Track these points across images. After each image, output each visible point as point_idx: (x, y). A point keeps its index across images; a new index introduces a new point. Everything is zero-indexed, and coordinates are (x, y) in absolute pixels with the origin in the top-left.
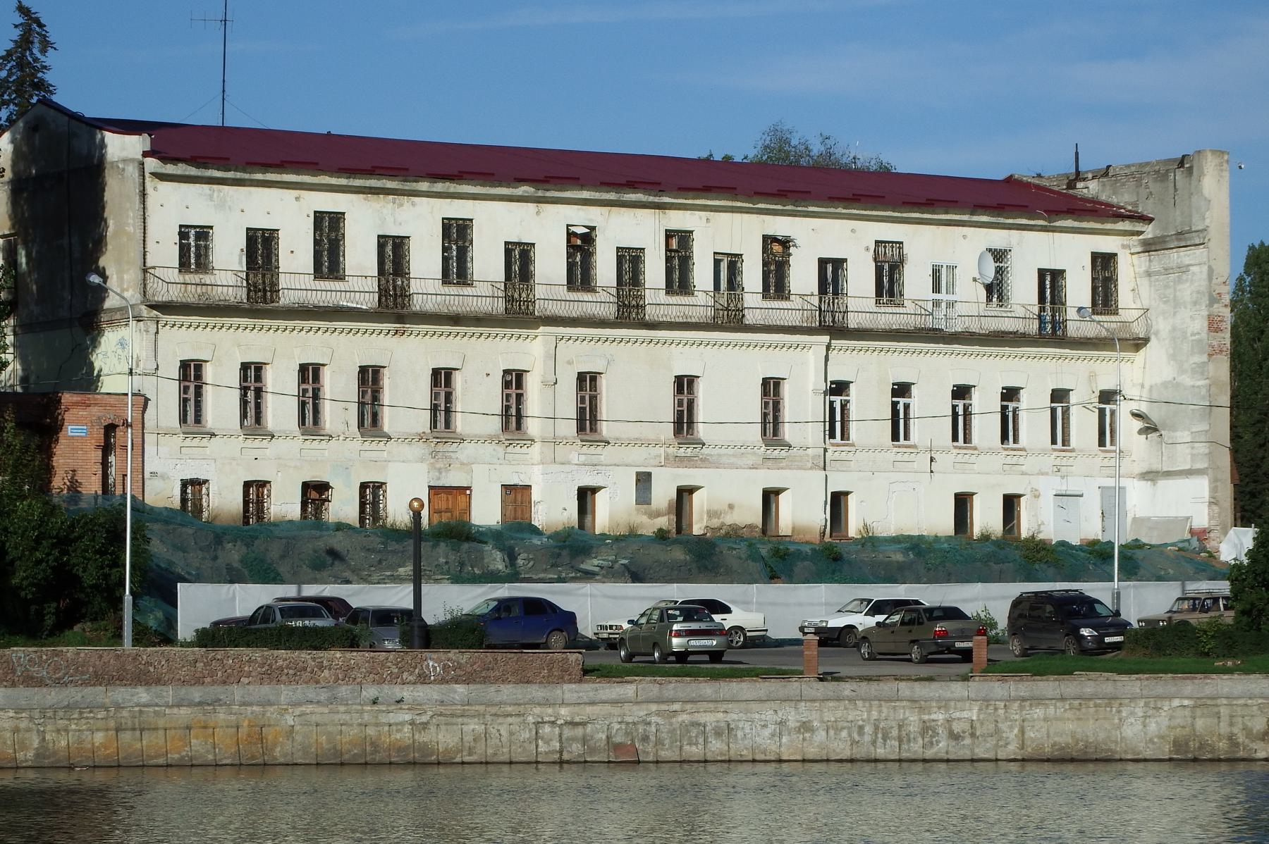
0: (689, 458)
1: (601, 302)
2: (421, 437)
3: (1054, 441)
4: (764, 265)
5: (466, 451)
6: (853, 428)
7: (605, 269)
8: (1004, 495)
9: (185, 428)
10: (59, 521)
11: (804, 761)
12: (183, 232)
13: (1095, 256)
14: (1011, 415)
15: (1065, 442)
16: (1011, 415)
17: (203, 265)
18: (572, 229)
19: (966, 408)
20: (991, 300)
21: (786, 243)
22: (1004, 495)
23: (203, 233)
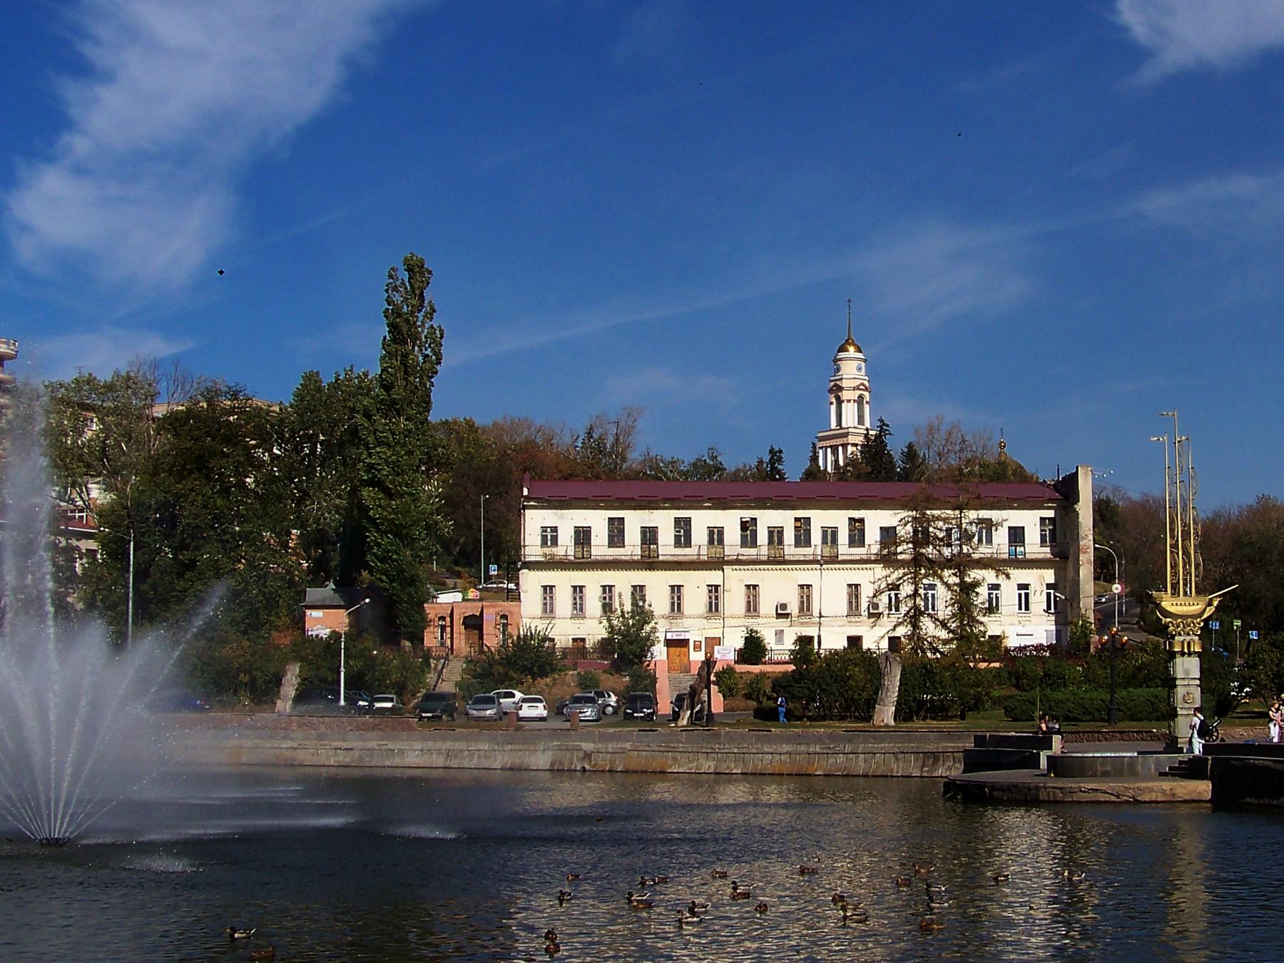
0: (807, 623)
1: (763, 550)
2: (700, 617)
3: (1020, 609)
4: (850, 530)
5: (686, 623)
6: (1032, 606)
7: (762, 537)
8: (848, 637)
9: (672, 614)
10: (856, 669)
11: (847, 776)
12: (544, 529)
13: (1041, 518)
14: (930, 599)
15: (1027, 608)
16: (930, 599)
17: (555, 542)
18: (744, 520)
19: (933, 595)
20: (460, 572)
21: (862, 521)
22: (848, 637)
23: (555, 529)
